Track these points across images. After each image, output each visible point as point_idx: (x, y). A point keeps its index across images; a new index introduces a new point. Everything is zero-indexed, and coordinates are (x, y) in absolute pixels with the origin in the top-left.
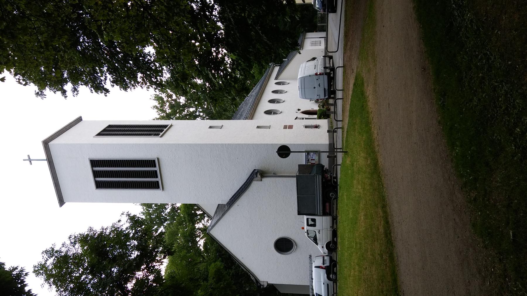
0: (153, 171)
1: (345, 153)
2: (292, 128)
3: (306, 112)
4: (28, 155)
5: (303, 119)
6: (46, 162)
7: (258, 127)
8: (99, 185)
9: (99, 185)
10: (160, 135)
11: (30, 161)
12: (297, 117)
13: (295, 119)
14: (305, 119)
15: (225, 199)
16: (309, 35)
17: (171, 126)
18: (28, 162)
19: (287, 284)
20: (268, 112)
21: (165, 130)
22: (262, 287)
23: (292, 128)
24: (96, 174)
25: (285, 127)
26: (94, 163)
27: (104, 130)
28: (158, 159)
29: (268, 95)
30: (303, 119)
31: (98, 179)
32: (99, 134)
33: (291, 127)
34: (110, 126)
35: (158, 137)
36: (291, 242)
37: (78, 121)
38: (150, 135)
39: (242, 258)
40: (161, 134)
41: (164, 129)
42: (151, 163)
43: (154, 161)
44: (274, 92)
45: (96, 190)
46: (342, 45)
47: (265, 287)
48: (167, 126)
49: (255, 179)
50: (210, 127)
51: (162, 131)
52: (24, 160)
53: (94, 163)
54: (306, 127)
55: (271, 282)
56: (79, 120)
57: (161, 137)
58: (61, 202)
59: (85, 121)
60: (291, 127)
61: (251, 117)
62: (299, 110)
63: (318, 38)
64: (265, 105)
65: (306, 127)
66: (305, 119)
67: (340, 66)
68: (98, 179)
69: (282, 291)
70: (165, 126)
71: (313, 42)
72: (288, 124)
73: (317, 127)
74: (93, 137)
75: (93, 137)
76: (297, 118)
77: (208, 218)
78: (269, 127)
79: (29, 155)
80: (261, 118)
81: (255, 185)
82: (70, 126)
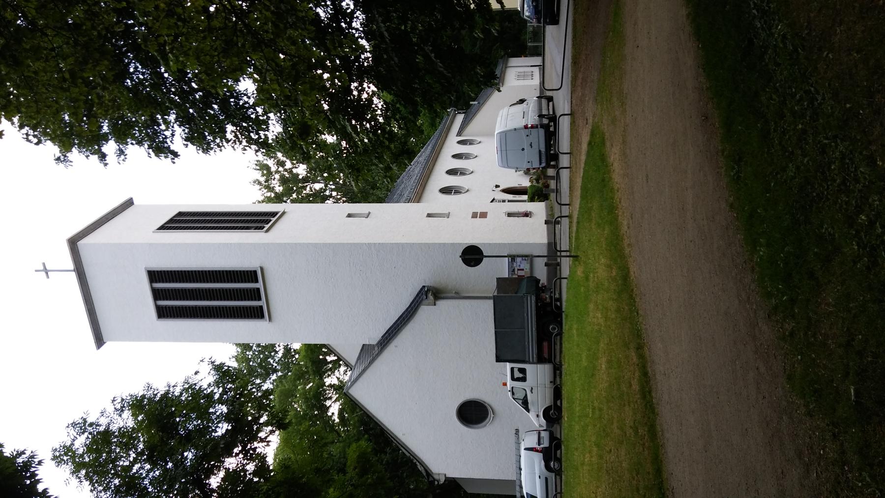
0: (254, 289)
5: (504, 201)
6: (74, 273)
7: (429, 215)
8: (163, 313)
9: (163, 313)
10: (265, 229)
13: (492, 202)
15: (374, 336)
16: (514, 61)
17: (284, 213)
20: (446, 191)
21: (274, 219)
24: (158, 295)
25: (475, 215)
26: (154, 276)
27: (171, 221)
28: (262, 269)
29: (446, 161)
30: (504, 201)
33: (484, 215)
34: (180, 214)
35: (263, 232)
40: (267, 226)
41: (271, 219)
42: (250, 276)
43: (255, 272)
47: (441, 483)
48: (276, 213)
49: (424, 302)
51: (268, 222)
53: (154, 276)
54: (510, 215)
55: (452, 474)
56: (129, 203)
58: (100, 341)
60: (484, 215)
62: (497, 186)
63: (528, 66)
64: (440, 178)
65: (510, 215)
66: (507, 201)
69: (470, 490)
70: (274, 214)
72: (479, 211)
74: (153, 232)
76: (495, 201)
78: (429, 215)
80: (434, 200)
81: (425, 311)
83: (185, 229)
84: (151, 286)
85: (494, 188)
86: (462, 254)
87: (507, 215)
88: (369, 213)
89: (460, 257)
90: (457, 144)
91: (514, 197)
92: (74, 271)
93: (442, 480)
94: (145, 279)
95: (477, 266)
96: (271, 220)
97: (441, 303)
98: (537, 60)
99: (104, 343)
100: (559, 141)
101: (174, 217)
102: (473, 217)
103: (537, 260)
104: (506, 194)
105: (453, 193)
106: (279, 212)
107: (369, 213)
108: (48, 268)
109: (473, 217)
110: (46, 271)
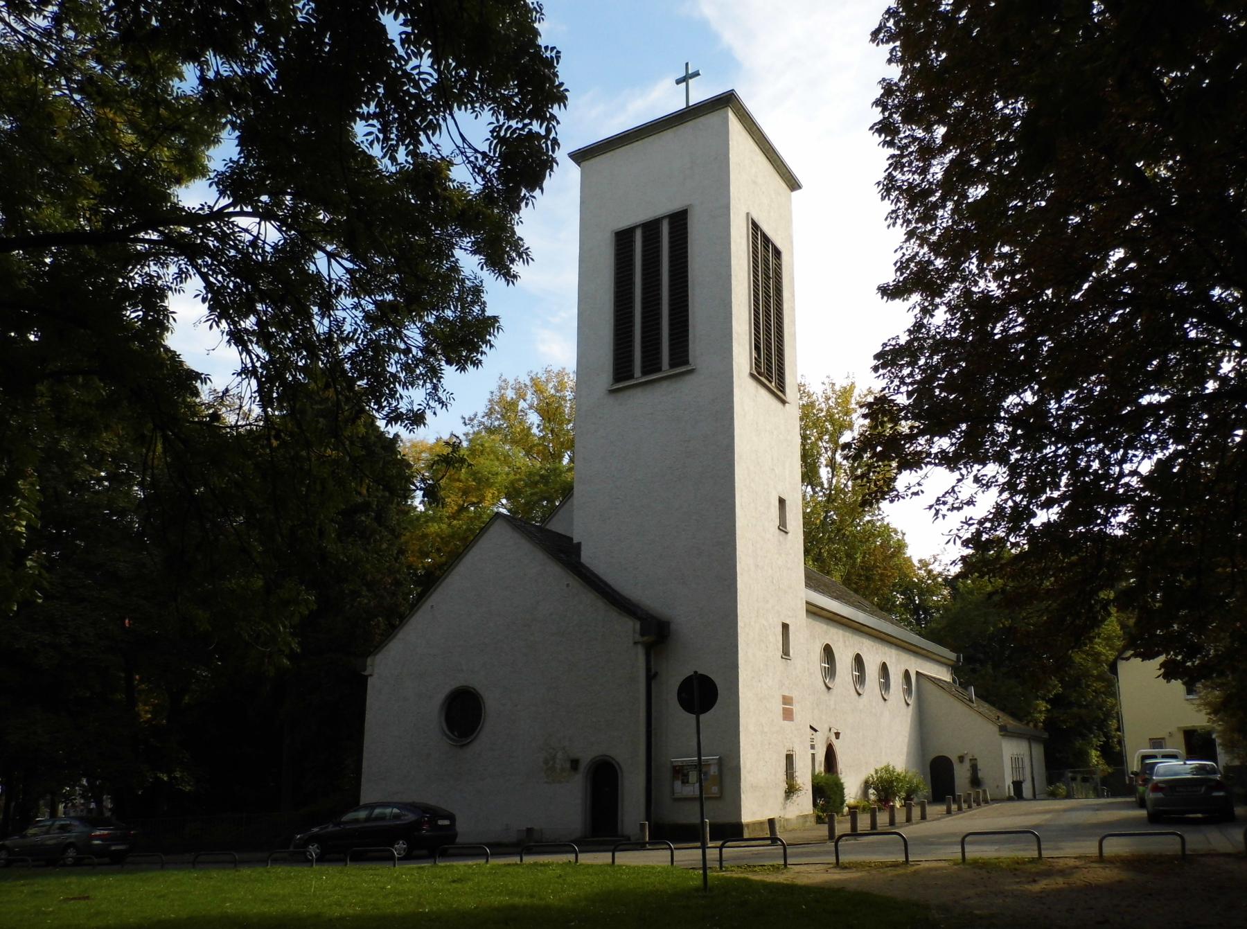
0: (660, 363)
1: (702, 877)
2: (785, 719)
3: (830, 757)
4: (700, 72)
5: (813, 747)
6: (685, 106)
7: (785, 627)
8: (623, 239)
11: (684, 80)
12: (816, 731)
13: (811, 727)
14: (812, 751)
16: (1038, 751)
17: (784, 402)
20: (828, 652)
21: (773, 386)
23: (785, 719)
24: (651, 228)
25: (787, 700)
26: (679, 220)
27: (766, 240)
28: (691, 371)
29: (874, 655)
30: (813, 747)
31: (638, 235)
32: (755, 226)
33: (788, 715)
34: (778, 253)
35: (751, 369)
36: (613, 766)
37: (789, 181)
38: (757, 348)
39: (432, 607)
41: (773, 384)
42: (680, 355)
43: (686, 362)
44: (884, 669)
48: (783, 392)
50: (782, 502)
52: (687, 64)
53: (679, 220)
54: (789, 758)
56: (793, 184)
59: (790, 196)
60: (788, 715)
61: (815, 609)
62: (837, 735)
63: (1032, 773)
64: (846, 646)
65: (789, 758)
66: (812, 751)
67: (1043, 852)
68: (638, 235)
70: (781, 386)
71: (1020, 760)
73: (782, 527)
74: (748, 214)
76: (814, 732)
77: (356, 300)
78: (785, 627)
79: (699, 74)
81: (628, 627)
82: (775, 161)
83: (783, 364)
84: (663, 218)
85: (834, 730)
86: (701, 675)
87: (789, 753)
88: (786, 533)
89: (696, 672)
90: (903, 671)
91: (821, 764)
94: (675, 206)
95: (681, 705)
96: (771, 382)
100: (747, 307)
101: (773, 244)
104: (825, 749)
105: (823, 665)
106: (785, 395)
108: (690, 81)
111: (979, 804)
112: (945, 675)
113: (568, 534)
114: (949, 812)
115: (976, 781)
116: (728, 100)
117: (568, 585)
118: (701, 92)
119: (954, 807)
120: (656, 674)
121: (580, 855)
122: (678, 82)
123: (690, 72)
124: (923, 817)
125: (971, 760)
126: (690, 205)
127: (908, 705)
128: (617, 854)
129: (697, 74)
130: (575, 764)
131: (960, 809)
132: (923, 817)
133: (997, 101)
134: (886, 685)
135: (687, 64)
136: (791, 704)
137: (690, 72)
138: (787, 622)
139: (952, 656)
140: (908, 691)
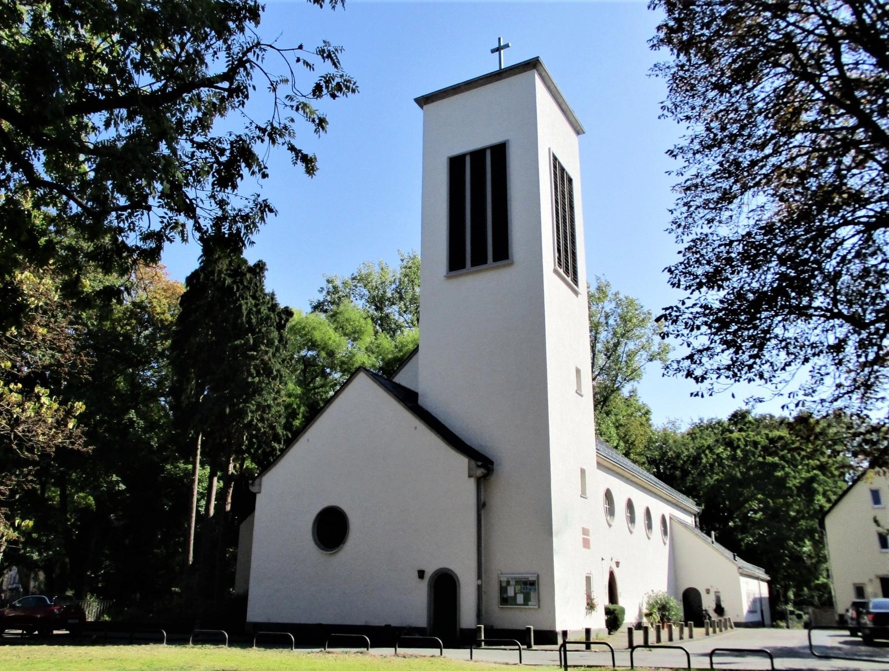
8: (456, 164)
9: (456, 164)
10: (559, 269)
15: (429, 399)
17: (576, 293)
18: (497, 46)
19: (255, 533)
20: (608, 495)
21: (569, 279)
22: (250, 482)
26: (500, 151)
27: (563, 170)
29: (642, 501)
32: (555, 159)
35: (555, 265)
38: (559, 250)
39: (308, 440)
40: (561, 271)
44: (648, 512)
45: (448, 277)
46: (361, 653)
47: (250, 488)
48: (577, 284)
49: (473, 462)
51: (567, 271)
53: (500, 151)
55: (260, 500)
57: (555, 271)
58: (423, 101)
62: (618, 564)
64: (623, 491)
69: (243, 527)
70: (575, 280)
72: (591, 538)
73: (579, 393)
74: (549, 149)
75: (549, 149)
78: (583, 472)
80: (602, 481)
81: (462, 462)
85: (615, 560)
92: (500, 68)
93: (253, 489)
97: (471, 484)
98: (767, 620)
99: (422, 107)
102: (584, 529)
103: (642, 643)
107: (582, 396)
109: (584, 529)
110: (498, 50)
111: (726, 629)
112: (690, 520)
113: (416, 391)
114: (707, 634)
115: (719, 610)
116: (533, 64)
117: (416, 428)
118: (509, 59)
119: (711, 630)
120: (484, 505)
121: (443, 650)
122: (493, 51)
123: (502, 44)
124: (691, 636)
125: (716, 592)
126: (508, 141)
127: (665, 544)
128: (807, 643)
129: (507, 46)
130: (421, 574)
131: (714, 632)
132: (691, 636)
133: (40, 554)
134: (649, 526)
135: (499, 39)
136: (588, 535)
137: (502, 44)
138: (584, 468)
139: (696, 509)
140: (665, 532)
